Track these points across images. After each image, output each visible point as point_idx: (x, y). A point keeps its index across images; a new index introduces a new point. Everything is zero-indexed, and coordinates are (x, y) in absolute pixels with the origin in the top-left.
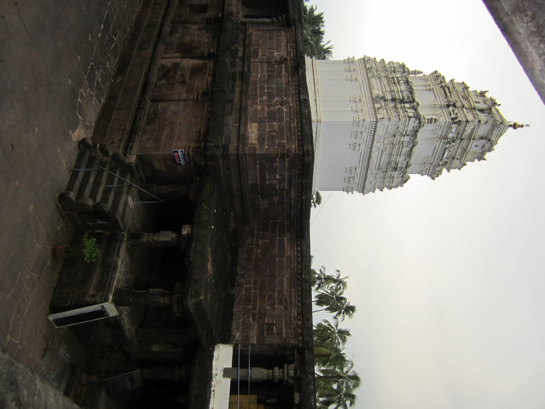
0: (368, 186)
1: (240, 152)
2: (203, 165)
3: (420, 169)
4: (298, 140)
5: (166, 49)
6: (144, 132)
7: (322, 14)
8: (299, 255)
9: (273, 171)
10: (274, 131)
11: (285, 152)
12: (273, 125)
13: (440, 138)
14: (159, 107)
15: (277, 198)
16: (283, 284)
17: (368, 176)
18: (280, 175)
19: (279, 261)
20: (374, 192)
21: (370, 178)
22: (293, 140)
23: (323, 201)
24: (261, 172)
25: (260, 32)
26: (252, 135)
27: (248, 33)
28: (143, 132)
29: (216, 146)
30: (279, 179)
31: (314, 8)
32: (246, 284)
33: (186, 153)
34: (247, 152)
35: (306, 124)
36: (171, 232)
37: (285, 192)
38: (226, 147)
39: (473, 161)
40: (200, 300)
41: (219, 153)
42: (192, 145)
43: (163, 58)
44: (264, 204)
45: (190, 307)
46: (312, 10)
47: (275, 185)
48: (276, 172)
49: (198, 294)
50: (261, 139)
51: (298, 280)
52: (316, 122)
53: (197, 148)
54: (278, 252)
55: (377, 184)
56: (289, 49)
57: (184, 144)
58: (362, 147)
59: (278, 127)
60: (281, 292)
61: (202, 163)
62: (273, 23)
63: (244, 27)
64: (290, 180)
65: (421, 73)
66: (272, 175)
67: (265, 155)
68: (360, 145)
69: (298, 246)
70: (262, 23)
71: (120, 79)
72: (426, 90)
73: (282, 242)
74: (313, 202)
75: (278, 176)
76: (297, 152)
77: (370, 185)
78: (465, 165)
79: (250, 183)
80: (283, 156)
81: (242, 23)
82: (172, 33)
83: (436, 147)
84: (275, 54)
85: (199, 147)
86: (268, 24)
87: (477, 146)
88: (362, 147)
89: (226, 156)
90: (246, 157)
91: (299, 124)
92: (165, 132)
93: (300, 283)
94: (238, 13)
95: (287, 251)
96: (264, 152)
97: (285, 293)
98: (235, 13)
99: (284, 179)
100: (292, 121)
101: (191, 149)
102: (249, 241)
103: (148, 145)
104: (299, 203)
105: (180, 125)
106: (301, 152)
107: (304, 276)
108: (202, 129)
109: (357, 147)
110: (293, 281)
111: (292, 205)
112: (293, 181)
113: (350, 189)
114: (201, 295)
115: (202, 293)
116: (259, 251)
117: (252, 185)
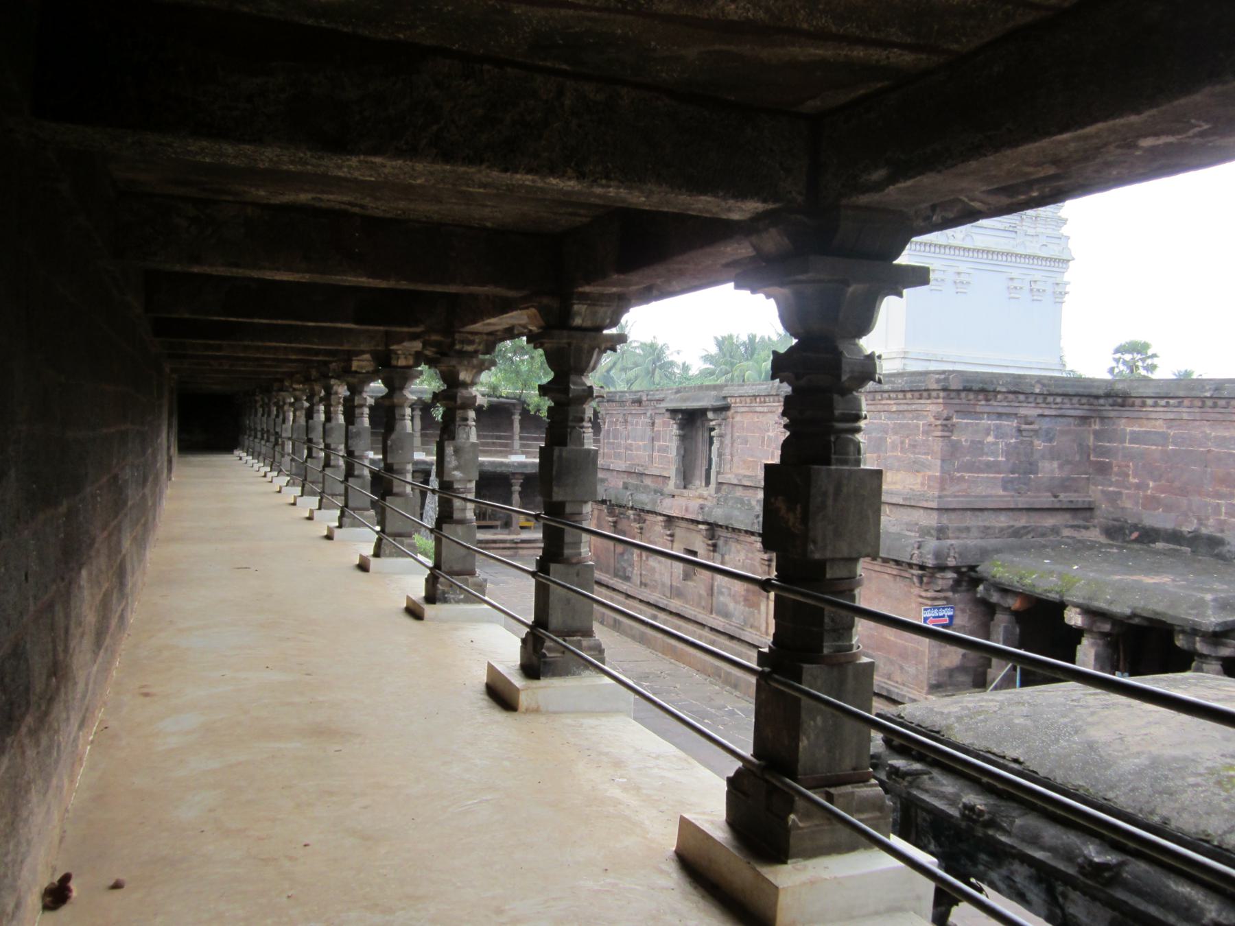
0: (1053, 251)
1: (934, 505)
2: (955, 575)
4: (920, 398)
5: (752, 627)
7: (716, 338)
8: (1163, 402)
9: (977, 447)
10: (902, 443)
11: (939, 422)
12: (892, 442)
15: (1036, 442)
16: (1225, 437)
17: (1029, 252)
18: (988, 434)
20: (1068, 238)
21: (1033, 248)
22: (919, 407)
23: (1140, 338)
24: (980, 471)
27: (735, 482)
28: (889, 679)
29: (919, 548)
30: (996, 437)
31: (704, 353)
32: (1219, 513)
33: (929, 602)
34: (936, 493)
35: (893, 383)
36: (1079, 647)
37: (1024, 427)
38: (925, 532)
40: (1215, 600)
41: (932, 544)
42: (916, 590)
44: (1049, 469)
45: (1220, 620)
46: (707, 358)
47: (1007, 445)
48: (981, 442)
49: (1201, 604)
50: (915, 467)
51: (1215, 406)
52: (906, 361)
53: (921, 582)
55: (1049, 232)
56: (766, 409)
57: (914, 605)
58: (963, 267)
59: (896, 433)
61: (951, 575)
63: (725, 487)
64: (1000, 415)
66: (986, 450)
67: (943, 460)
68: (959, 273)
69: (1144, 405)
70: (720, 455)
73: (1136, 438)
74: (1143, 360)
75: (990, 439)
76: (941, 401)
77: (1050, 246)
79: (1001, 493)
80: (948, 427)
81: (718, 490)
82: (726, 615)
84: (771, 434)
85: (921, 578)
86: (721, 443)
88: (963, 267)
89: (941, 532)
90: (946, 496)
91: (893, 395)
92: (892, 638)
93: (1222, 403)
94: (701, 497)
95: (1154, 427)
96: (939, 462)
98: (701, 501)
99: (998, 427)
100: (886, 408)
101: (924, 594)
102: (1128, 505)
103: (912, 670)
104: (1050, 399)
106: (942, 394)
107: (1208, 394)
108: (889, 571)
109: (963, 278)
110: (1219, 416)
111: (1054, 413)
112: (1000, 410)
113: (1058, 289)
114: (1202, 599)
115: (1200, 595)
116: (1151, 484)
117: (1005, 489)
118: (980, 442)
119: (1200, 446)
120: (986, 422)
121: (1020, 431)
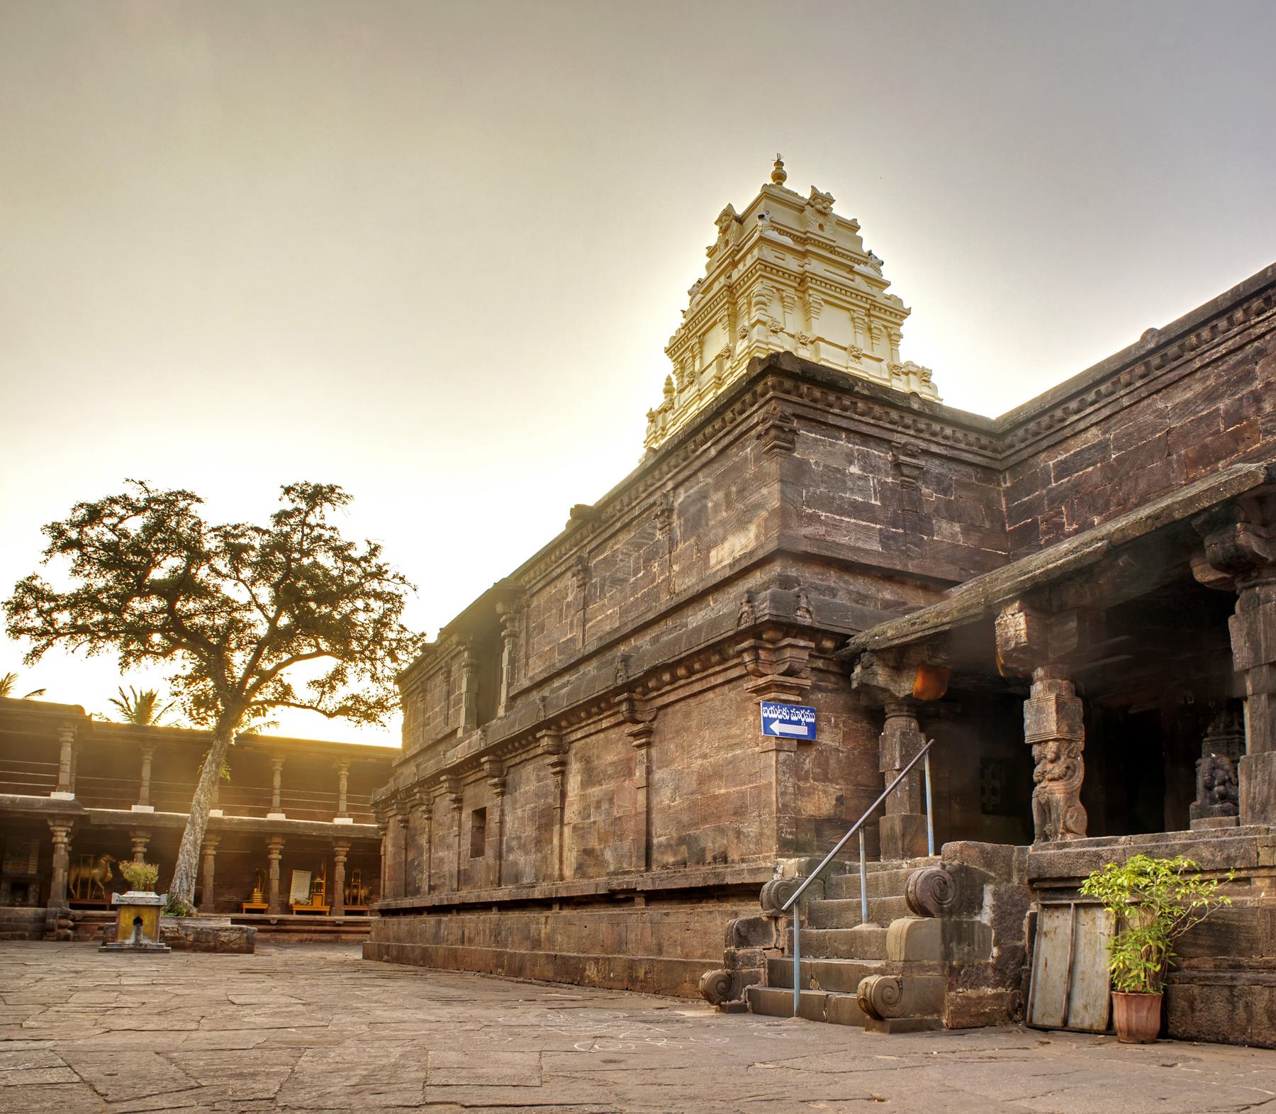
3: (884, 341)
6: (724, 858)
9: (836, 477)
13: (804, 292)
14: (663, 839)
18: (851, 463)
19: (1118, 449)
25: (531, 661)
26: (738, 548)
39: (860, 240)
43: (562, 878)
54: (1094, 464)
60: (1210, 396)
62: (514, 635)
65: (669, 378)
66: (850, 484)
70: (512, 661)
71: (591, 972)
72: (701, 352)
75: (854, 469)
78: (870, 253)
83: (825, 301)
87: (821, 226)
92: (723, 791)
97: (1211, 382)
105: (705, 756)
118: (838, 470)
119: (1153, 433)
120: (843, 443)
121: (897, 465)
